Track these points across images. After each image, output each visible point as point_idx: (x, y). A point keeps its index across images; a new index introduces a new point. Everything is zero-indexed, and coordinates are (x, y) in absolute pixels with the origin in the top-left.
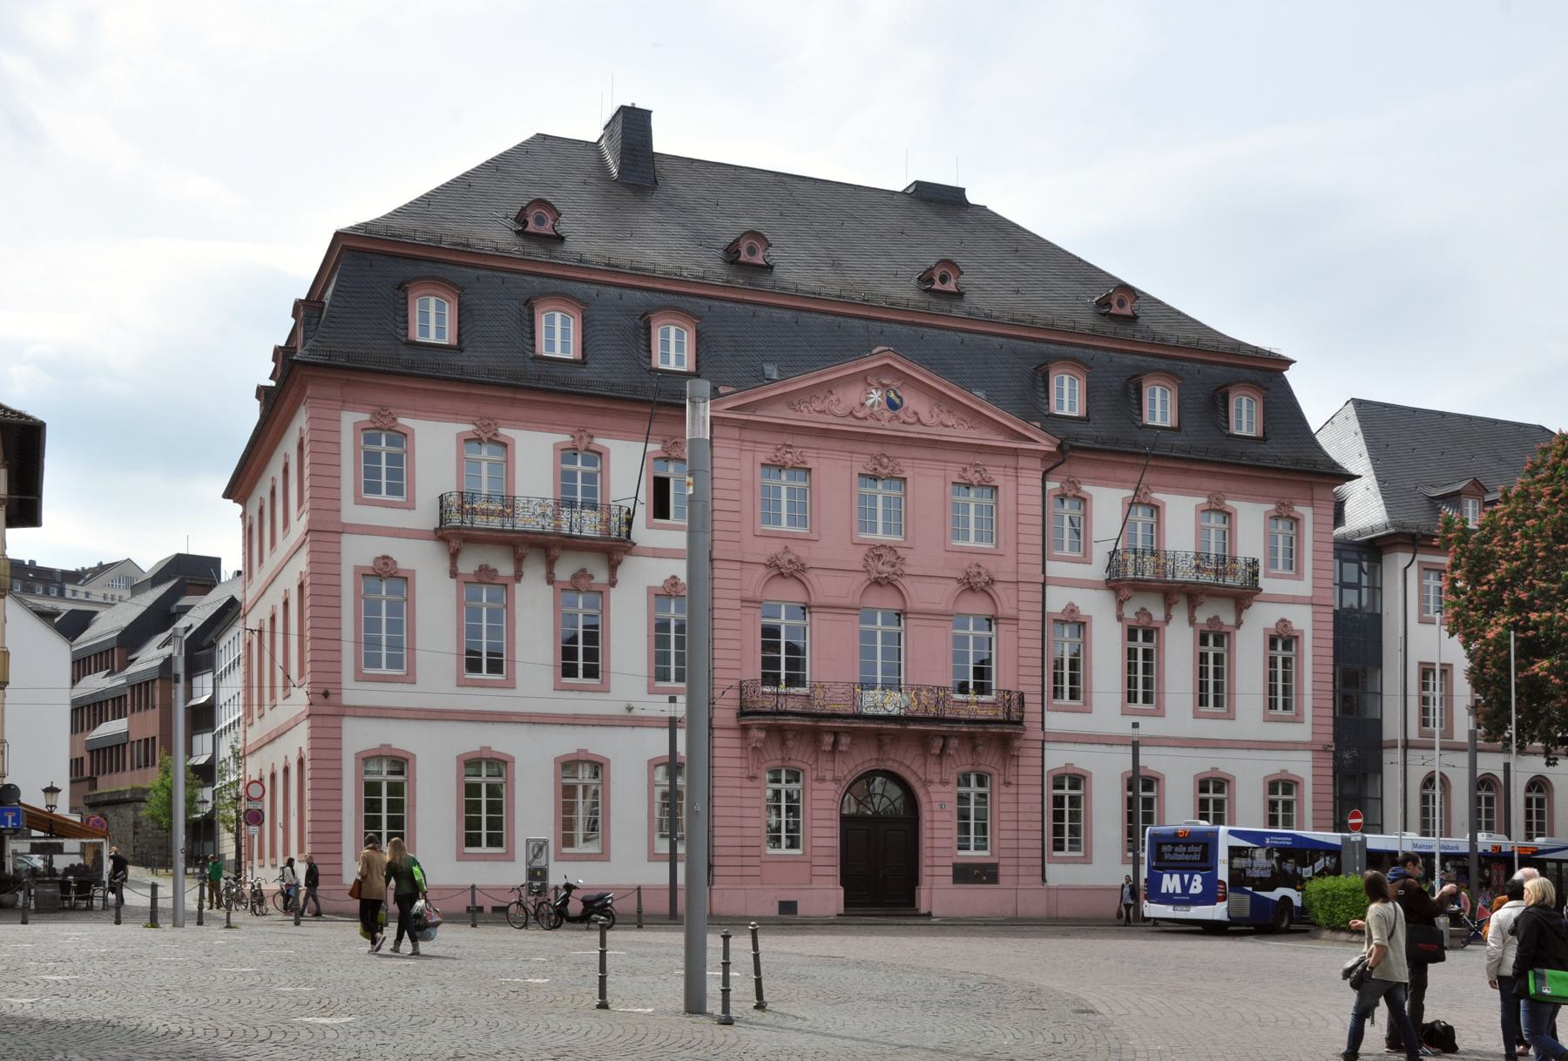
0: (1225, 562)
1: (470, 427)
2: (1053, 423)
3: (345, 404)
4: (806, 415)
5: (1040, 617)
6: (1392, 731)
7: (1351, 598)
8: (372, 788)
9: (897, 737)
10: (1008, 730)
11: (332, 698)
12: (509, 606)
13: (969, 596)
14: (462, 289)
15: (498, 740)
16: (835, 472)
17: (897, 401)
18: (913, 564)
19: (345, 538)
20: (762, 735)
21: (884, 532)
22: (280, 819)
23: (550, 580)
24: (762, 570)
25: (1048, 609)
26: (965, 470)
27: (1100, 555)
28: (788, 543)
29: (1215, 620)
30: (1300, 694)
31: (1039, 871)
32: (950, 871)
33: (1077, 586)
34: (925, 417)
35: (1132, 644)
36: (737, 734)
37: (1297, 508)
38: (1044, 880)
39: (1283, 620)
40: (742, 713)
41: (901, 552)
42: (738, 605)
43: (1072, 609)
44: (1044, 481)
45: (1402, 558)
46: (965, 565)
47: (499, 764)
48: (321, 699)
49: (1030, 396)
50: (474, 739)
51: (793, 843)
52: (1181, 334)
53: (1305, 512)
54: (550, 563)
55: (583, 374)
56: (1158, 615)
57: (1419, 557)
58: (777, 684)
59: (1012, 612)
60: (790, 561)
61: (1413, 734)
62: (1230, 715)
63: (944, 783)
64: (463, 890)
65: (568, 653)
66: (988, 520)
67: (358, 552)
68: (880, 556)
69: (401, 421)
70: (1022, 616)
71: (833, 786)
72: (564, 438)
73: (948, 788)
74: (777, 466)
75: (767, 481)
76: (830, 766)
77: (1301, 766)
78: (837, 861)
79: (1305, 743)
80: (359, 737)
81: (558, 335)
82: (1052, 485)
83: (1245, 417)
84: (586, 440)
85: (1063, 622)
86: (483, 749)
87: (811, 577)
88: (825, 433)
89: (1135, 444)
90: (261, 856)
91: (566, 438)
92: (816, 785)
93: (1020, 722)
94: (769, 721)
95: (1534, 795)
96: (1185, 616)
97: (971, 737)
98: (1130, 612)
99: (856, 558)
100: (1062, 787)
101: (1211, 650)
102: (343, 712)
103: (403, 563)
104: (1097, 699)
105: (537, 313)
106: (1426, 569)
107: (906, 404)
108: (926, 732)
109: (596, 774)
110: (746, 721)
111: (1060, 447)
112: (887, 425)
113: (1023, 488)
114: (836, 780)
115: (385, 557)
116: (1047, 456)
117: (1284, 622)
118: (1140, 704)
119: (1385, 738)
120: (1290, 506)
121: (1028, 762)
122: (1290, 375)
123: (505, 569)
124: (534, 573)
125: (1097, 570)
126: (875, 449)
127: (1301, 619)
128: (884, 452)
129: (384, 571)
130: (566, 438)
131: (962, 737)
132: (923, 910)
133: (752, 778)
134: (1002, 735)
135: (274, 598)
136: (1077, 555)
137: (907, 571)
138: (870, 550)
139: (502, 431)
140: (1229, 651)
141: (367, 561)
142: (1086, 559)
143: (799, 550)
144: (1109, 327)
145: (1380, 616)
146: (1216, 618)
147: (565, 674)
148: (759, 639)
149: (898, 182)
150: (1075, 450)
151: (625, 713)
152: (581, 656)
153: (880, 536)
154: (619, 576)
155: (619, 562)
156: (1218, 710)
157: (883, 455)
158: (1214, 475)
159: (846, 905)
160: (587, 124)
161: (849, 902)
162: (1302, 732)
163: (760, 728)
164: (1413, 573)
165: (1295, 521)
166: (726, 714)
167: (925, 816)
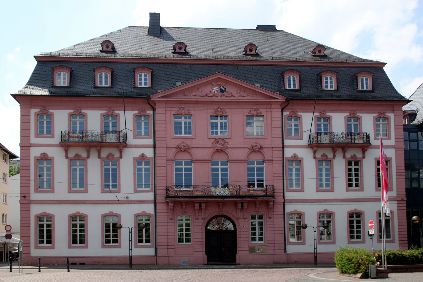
2: (284, 92)
3: (32, 107)
4: (191, 97)
5: (281, 159)
9: (225, 204)
11: (27, 198)
12: (332, 167)
14: (301, 72)
15: (82, 209)
17: (224, 89)
18: (231, 144)
23: (99, 157)
25: (285, 156)
27: (306, 136)
28: (183, 140)
32: (248, 249)
33: (297, 147)
35: (350, 167)
36: (166, 205)
37: (387, 114)
40: (167, 197)
43: (295, 156)
44: (282, 111)
47: (359, 215)
50: (73, 209)
51: (188, 241)
52: (342, 58)
53: (391, 116)
55: (338, 94)
58: (254, 186)
60: (184, 146)
62: (362, 190)
68: (218, 142)
69: (50, 111)
71: (202, 221)
73: (247, 220)
74: (178, 115)
75: (176, 120)
76: (242, 214)
78: (204, 246)
79: (34, 203)
80: (36, 210)
81: (330, 83)
82: (286, 114)
83: (365, 84)
84: (111, 112)
85: (293, 160)
86: (77, 212)
87: (193, 151)
88: (197, 103)
89: (333, 97)
91: (105, 112)
93: (273, 196)
94: (173, 200)
96: (97, 154)
98: (318, 156)
99: (209, 144)
100: (353, 217)
101: (353, 167)
102: (30, 202)
103: (50, 155)
104: (90, 188)
105: (285, 76)
107: (227, 90)
108: (238, 201)
110: (169, 200)
111: (286, 100)
112: (220, 98)
116: (282, 104)
117: (143, 155)
120: (384, 113)
121: (278, 210)
122: (385, 69)
124: (94, 155)
125: (305, 141)
126: (216, 106)
127: (391, 154)
128: (219, 108)
129: (44, 158)
130: (105, 112)
137: (229, 146)
138: (215, 140)
139: (83, 111)
140: (360, 167)
141: (38, 155)
142: (301, 138)
143: (189, 143)
144: (317, 59)
146: (354, 155)
148: (247, 172)
150: (293, 101)
153: (219, 135)
156: (357, 188)
158: (352, 105)
161: (208, 261)
163: (171, 202)
165: (388, 118)
166: (161, 198)
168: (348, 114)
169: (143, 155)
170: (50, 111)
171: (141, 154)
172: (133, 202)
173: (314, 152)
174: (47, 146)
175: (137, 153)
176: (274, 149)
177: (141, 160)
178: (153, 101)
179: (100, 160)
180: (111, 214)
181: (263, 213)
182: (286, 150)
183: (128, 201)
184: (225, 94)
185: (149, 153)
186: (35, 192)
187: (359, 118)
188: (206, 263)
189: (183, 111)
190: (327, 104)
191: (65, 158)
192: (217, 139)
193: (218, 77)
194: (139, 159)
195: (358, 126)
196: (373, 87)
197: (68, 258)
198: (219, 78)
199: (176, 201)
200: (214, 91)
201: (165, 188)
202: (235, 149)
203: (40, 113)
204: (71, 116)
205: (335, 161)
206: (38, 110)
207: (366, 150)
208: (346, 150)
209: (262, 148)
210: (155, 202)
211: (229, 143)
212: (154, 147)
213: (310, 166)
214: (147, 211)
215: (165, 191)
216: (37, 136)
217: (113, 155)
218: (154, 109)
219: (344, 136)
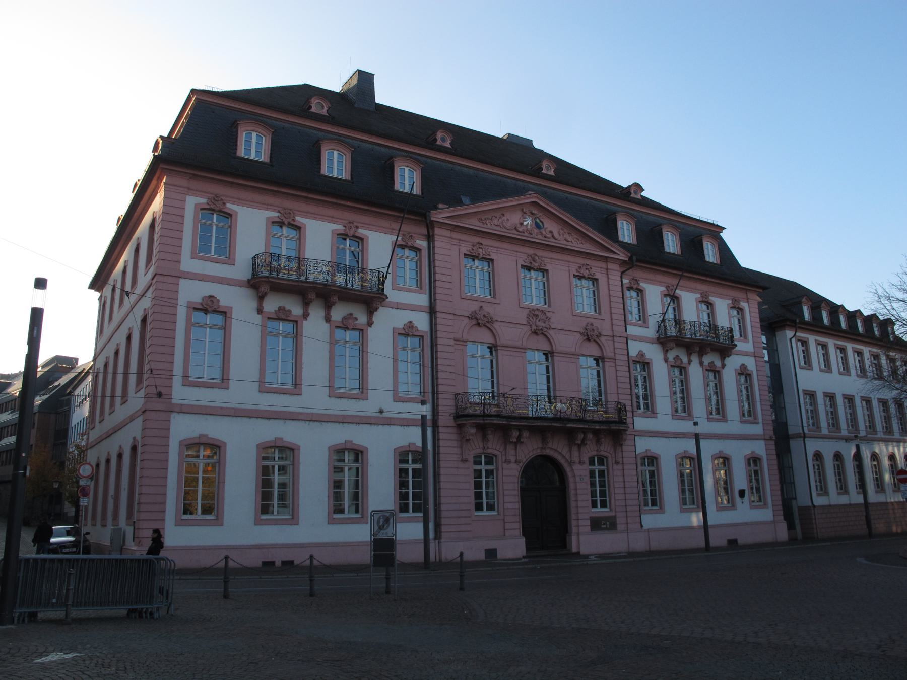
0: (713, 327)
1: (277, 214)
3: (190, 191)
8: (192, 470)
13: (587, 344)
15: (289, 432)
16: (508, 260)
19: (183, 283)
20: (473, 430)
22: (112, 491)
23: (328, 319)
24: (466, 321)
26: (580, 268)
27: (653, 321)
29: (712, 364)
31: (638, 519)
32: (588, 523)
33: (642, 342)
34: (556, 235)
36: (454, 430)
38: (642, 526)
39: (743, 365)
40: (457, 416)
41: (548, 314)
42: (452, 343)
43: (641, 354)
46: (584, 324)
49: (609, 228)
54: (328, 307)
56: (685, 359)
59: (611, 355)
60: (484, 316)
63: (581, 463)
69: (229, 205)
70: (618, 357)
72: (339, 227)
77: (760, 448)
80: (183, 428)
86: (201, 436)
88: (501, 238)
90: (94, 518)
92: (505, 466)
96: (322, 313)
99: (522, 317)
102: (173, 409)
103: (224, 302)
108: (567, 428)
109: (356, 460)
111: (630, 258)
113: (612, 279)
114: (517, 462)
115: (211, 296)
117: (410, 325)
123: (296, 310)
124: (316, 313)
128: (536, 254)
129: (209, 306)
132: (574, 550)
134: (614, 430)
141: (197, 299)
142: (230, 261)
145: (779, 365)
154: (374, 319)
155: (377, 309)
157: (535, 255)
159: (527, 549)
160: (334, 80)
162: (757, 429)
169: (410, 325)
174: (218, 282)
175: (400, 319)
176: (616, 339)
177: (408, 331)
180: (203, 440)
185: (422, 322)
191: (663, 362)
192: (534, 310)
193: (534, 200)
194: (200, 307)
195: (359, 256)
199: (489, 423)
202: (567, 333)
203: (208, 207)
206: (203, 201)
209: (600, 335)
211: (552, 320)
212: (432, 311)
213: (660, 372)
215: (453, 403)
216: (194, 256)
217: (356, 319)
218: (430, 238)
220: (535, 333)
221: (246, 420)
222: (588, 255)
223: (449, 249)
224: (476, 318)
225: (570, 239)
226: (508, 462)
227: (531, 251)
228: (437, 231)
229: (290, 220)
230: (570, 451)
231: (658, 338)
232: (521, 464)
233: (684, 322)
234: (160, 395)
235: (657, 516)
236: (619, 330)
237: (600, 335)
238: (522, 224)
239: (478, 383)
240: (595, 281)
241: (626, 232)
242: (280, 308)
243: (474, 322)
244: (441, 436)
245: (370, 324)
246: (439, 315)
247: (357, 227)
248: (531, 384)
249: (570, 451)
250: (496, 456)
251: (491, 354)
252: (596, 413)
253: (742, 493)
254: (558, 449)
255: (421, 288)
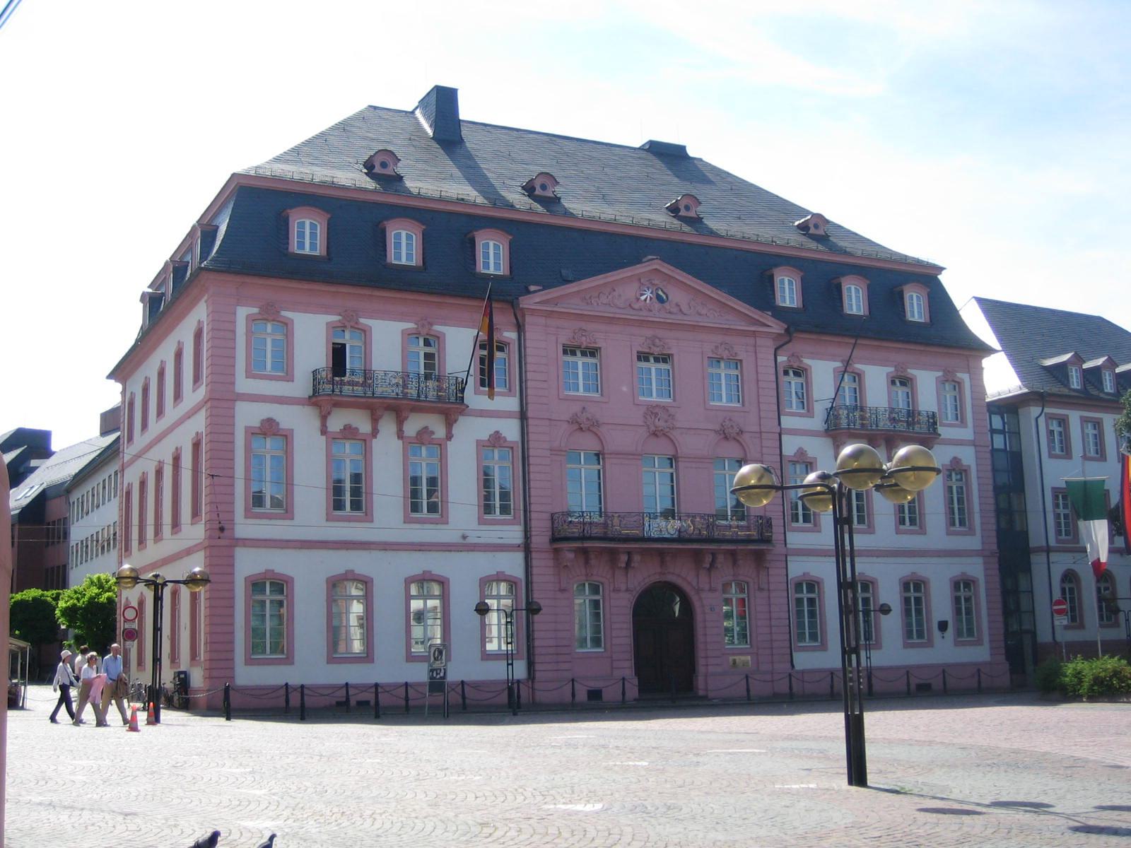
0: (912, 414)
2: (781, 313)
3: (239, 303)
6: (1036, 540)
7: (999, 442)
9: (676, 554)
10: (763, 547)
11: (226, 533)
20: (571, 555)
21: (658, 396)
23: (400, 435)
25: (784, 453)
26: (717, 347)
27: (820, 409)
30: (971, 513)
34: (685, 308)
37: (959, 375)
38: (793, 666)
39: (955, 458)
40: (555, 539)
41: (672, 411)
42: (548, 453)
43: (801, 452)
45: (1035, 411)
48: (217, 533)
49: (762, 295)
54: (400, 422)
57: (1046, 410)
60: (588, 419)
61: (1052, 542)
62: (369, 517)
63: (712, 590)
64: (282, 687)
65: (337, 489)
66: (738, 385)
67: (247, 415)
77: (975, 568)
80: (248, 564)
86: (267, 571)
88: (611, 320)
91: (410, 325)
94: (578, 544)
95: (1067, 586)
97: (733, 554)
103: (285, 424)
104: (378, 512)
106: (1050, 417)
107: (670, 298)
111: (787, 330)
113: (763, 360)
114: (627, 590)
117: (956, 461)
118: (907, 526)
119: (1031, 545)
122: (942, 278)
124: (388, 427)
127: (968, 456)
129: (269, 428)
131: (643, 552)
132: (701, 693)
133: (562, 590)
135: (164, 453)
136: (802, 411)
138: (648, 409)
141: (256, 423)
147: (900, 523)
149: (637, 143)
151: (461, 541)
152: (425, 497)
154: (454, 431)
155: (456, 421)
160: (406, 95)
163: (570, 550)
164: (1042, 421)
166: (541, 539)
167: (699, 617)
168: (892, 369)
170: (284, 313)
171: (492, 432)
172: (423, 548)
173: (324, 419)
177: (496, 440)
178: (522, 309)
179: (401, 442)
181: (601, 579)
182: (784, 438)
183: (465, 546)
184: (667, 305)
185: (511, 431)
186: (246, 517)
187: (438, 338)
188: (633, 692)
189: (584, 338)
190: (371, 296)
193: (654, 267)
194: (258, 431)
196: (423, 259)
197: (832, 673)
198: (656, 269)
199: (580, 545)
200: (643, 298)
201: (547, 516)
204: (406, 335)
205: (377, 444)
207: (456, 421)
208: (406, 418)
209: (741, 432)
210: (527, 548)
212: (523, 416)
214: (509, 572)
215: (549, 524)
217: (433, 433)
218: (520, 328)
219: (401, 383)
220: (655, 434)
221: (428, 552)
222: (727, 331)
223: (543, 341)
224: (577, 422)
225: (704, 312)
226: (617, 590)
227: (649, 333)
228: (528, 319)
229: (352, 324)
230: (698, 576)
231: (827, 430)
232: (634, 593)
233: (919, 414)
234: (222, 529)
235: (926, 650)
236: (770, 425)
237: (741, 432)
238: (638, 299)
239: (580, 497)
240: (738, 363)
241: (788, 292)
242: (345, 426)
243: (576, 427)
244: (535, 563)
245: (449, 437)
246: (530, 422)
247: (431, 324)
248: (649, 494)
249: (698, 576)
250: (602, 584)
251: (672, 467)
252: (731, 526)
253: (943, 626)
254: (682, 574)
255: (510, 390)
